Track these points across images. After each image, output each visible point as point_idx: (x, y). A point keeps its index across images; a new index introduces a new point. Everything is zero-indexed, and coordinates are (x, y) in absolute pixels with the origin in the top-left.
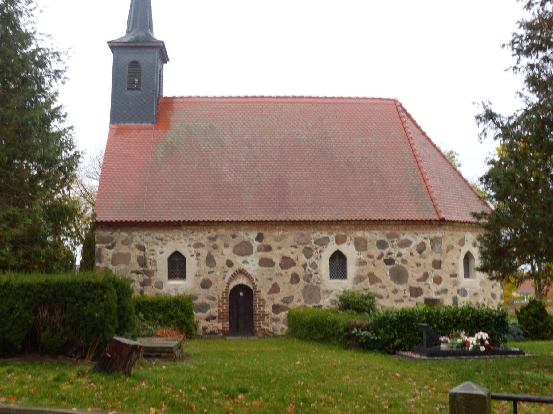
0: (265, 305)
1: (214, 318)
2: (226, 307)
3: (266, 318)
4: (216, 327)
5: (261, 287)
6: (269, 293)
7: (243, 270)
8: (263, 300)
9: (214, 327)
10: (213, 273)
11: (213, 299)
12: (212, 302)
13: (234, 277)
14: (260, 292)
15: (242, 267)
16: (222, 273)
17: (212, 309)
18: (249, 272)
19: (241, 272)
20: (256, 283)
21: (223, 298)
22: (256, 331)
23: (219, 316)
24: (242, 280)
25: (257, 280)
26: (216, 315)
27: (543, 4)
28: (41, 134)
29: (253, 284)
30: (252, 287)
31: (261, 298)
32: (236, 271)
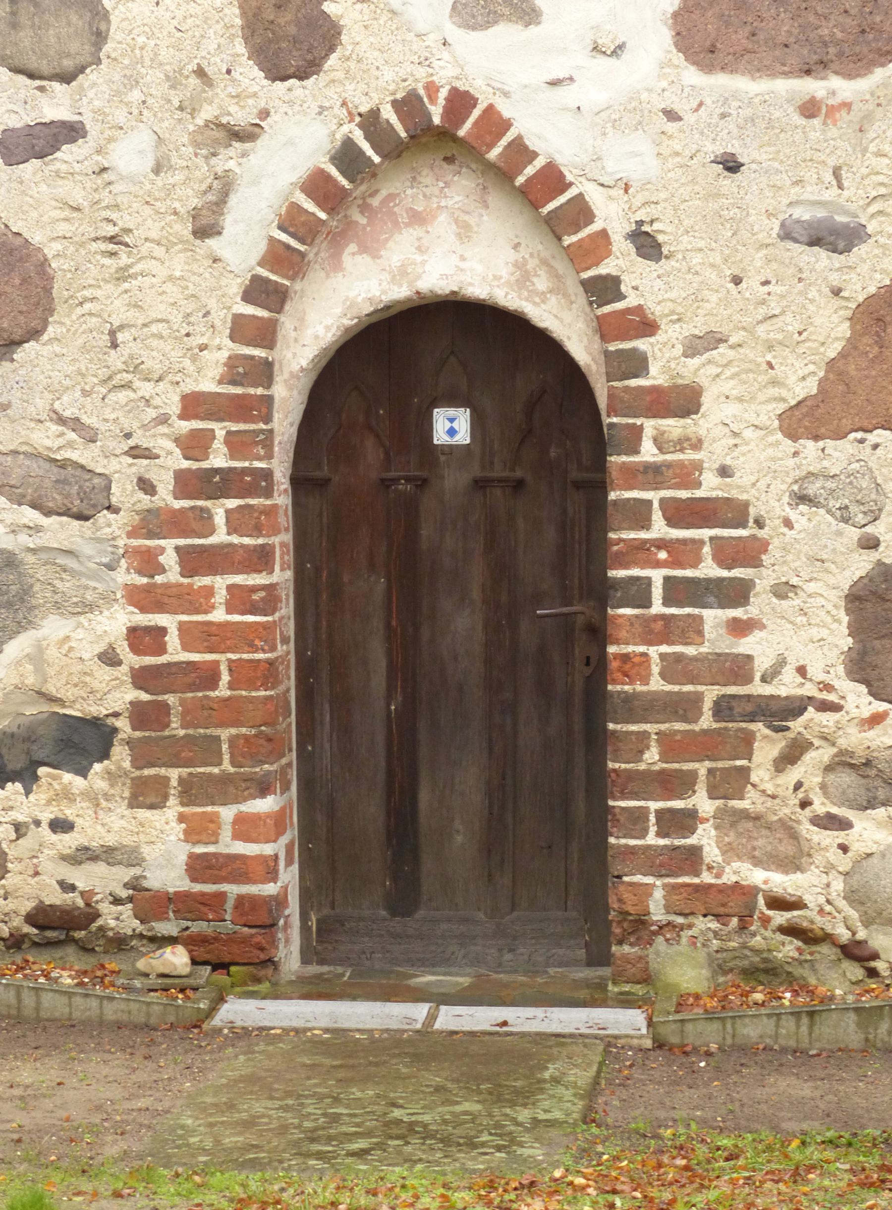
0: (763, 580)
1: (80, 741)
2: (250, 603)
3: (767, 747)
4: (107, 855)
5: (701, 344)
6: (806, 421)
7: (460, 102)
8: (732, 512)
9: (84, 855)
10: (68, 154)
11: (83, 499)
12: (61, 531)
13: (339, 200)
14: (683, 401)
15: (445, 75)
16: (184, 154)
17: (53, 628)
18: (549, 133)
19: (440, 135)
20: (643, 285)
21: (199, 484)
22: (639, 927)
23: (145, 716)
24: (451, 248)
25: (646, 244)
26: (113, 696)
27: (673, 1202)
28: (260, 706)
29: (604, 289)
30: (569, 326)
31: (710, 486)
32: (371, 122)
